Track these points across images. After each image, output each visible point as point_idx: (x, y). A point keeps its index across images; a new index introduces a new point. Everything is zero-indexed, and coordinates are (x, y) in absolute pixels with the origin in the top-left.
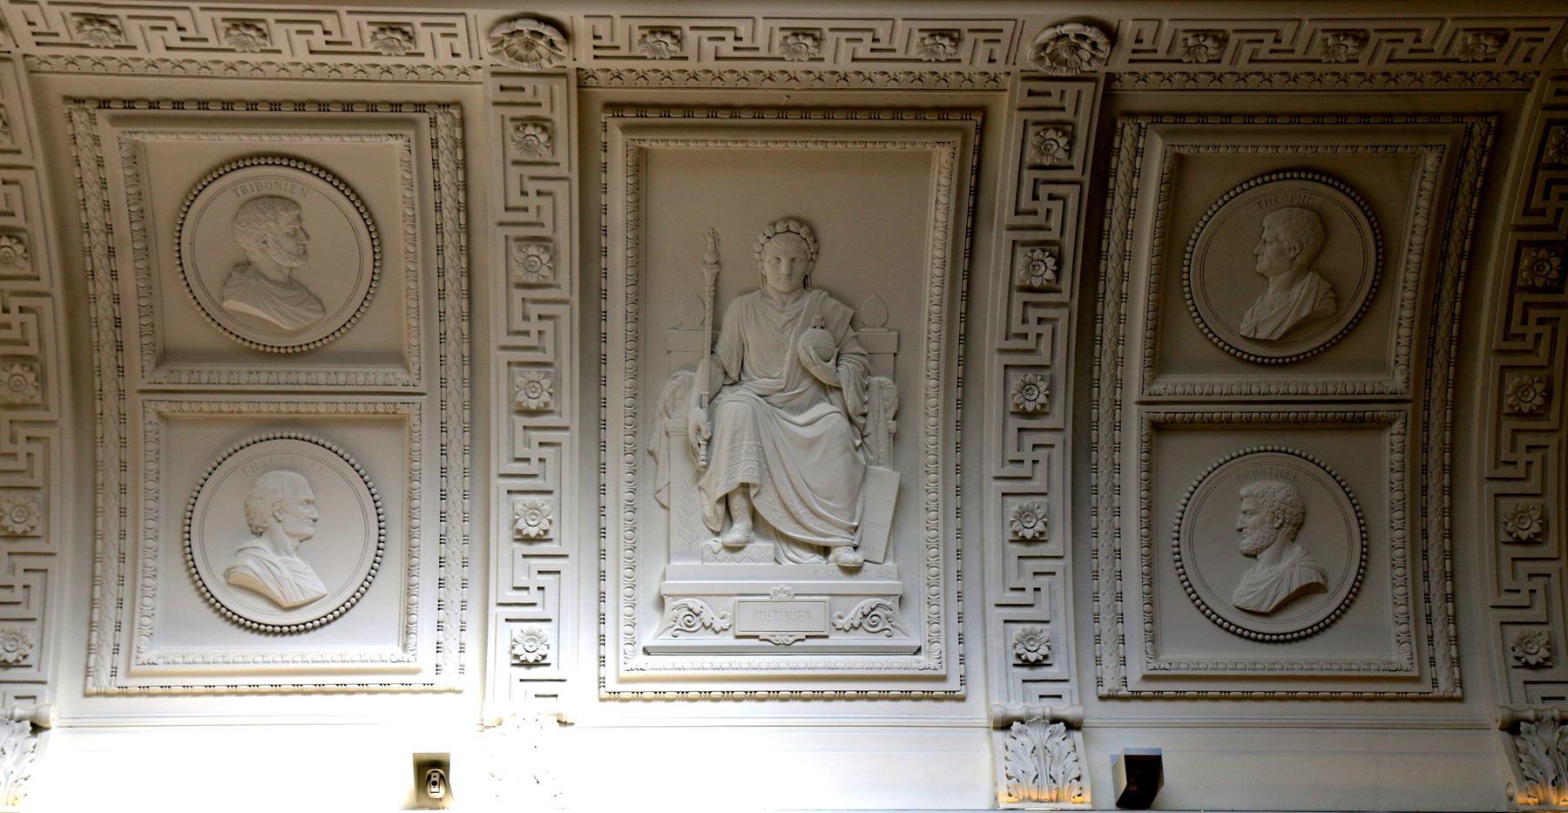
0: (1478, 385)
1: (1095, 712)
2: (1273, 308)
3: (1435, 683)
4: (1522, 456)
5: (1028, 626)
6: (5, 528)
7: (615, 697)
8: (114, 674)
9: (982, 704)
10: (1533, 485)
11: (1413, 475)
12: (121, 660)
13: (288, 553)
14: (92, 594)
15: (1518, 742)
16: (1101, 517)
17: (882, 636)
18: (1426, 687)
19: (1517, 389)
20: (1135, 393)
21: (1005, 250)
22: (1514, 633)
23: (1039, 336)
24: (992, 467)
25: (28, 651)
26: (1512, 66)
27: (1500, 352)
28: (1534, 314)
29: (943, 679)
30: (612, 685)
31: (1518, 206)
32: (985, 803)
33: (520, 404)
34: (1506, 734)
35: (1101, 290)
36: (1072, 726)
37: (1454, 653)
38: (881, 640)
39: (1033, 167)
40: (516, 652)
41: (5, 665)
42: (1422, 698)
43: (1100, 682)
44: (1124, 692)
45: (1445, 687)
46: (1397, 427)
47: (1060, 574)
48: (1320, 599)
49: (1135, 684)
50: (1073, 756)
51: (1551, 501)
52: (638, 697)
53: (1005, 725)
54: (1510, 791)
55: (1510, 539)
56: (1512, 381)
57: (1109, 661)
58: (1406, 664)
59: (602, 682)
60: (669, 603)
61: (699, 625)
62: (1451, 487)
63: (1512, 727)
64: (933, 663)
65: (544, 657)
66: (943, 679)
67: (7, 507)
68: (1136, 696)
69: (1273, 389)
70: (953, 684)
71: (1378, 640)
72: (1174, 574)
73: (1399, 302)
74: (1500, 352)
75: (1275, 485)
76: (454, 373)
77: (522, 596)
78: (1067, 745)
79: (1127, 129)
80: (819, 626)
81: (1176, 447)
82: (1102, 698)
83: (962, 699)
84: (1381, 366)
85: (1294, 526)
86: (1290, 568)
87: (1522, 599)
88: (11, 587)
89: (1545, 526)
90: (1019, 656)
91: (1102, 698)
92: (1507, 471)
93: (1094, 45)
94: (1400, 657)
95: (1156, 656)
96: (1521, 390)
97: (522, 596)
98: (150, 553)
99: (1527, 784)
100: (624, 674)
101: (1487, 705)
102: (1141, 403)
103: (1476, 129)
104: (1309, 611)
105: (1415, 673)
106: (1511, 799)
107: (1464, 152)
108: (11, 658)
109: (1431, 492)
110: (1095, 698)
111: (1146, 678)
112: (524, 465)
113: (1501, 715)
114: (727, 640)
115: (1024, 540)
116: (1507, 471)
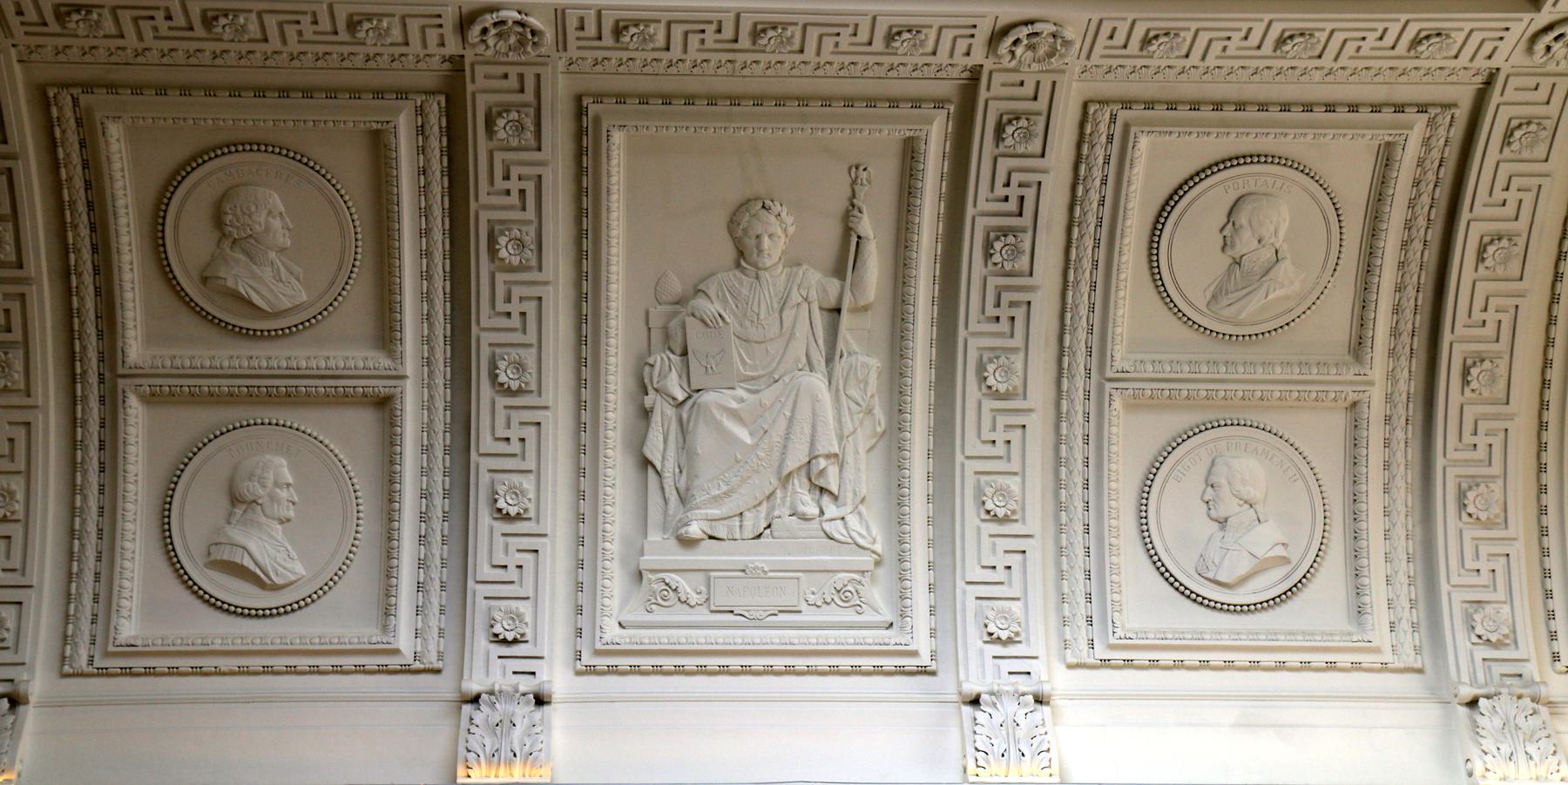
7: (591, 671)
18: (1387, 657)
30: (587, 659)
70: (924, 660)
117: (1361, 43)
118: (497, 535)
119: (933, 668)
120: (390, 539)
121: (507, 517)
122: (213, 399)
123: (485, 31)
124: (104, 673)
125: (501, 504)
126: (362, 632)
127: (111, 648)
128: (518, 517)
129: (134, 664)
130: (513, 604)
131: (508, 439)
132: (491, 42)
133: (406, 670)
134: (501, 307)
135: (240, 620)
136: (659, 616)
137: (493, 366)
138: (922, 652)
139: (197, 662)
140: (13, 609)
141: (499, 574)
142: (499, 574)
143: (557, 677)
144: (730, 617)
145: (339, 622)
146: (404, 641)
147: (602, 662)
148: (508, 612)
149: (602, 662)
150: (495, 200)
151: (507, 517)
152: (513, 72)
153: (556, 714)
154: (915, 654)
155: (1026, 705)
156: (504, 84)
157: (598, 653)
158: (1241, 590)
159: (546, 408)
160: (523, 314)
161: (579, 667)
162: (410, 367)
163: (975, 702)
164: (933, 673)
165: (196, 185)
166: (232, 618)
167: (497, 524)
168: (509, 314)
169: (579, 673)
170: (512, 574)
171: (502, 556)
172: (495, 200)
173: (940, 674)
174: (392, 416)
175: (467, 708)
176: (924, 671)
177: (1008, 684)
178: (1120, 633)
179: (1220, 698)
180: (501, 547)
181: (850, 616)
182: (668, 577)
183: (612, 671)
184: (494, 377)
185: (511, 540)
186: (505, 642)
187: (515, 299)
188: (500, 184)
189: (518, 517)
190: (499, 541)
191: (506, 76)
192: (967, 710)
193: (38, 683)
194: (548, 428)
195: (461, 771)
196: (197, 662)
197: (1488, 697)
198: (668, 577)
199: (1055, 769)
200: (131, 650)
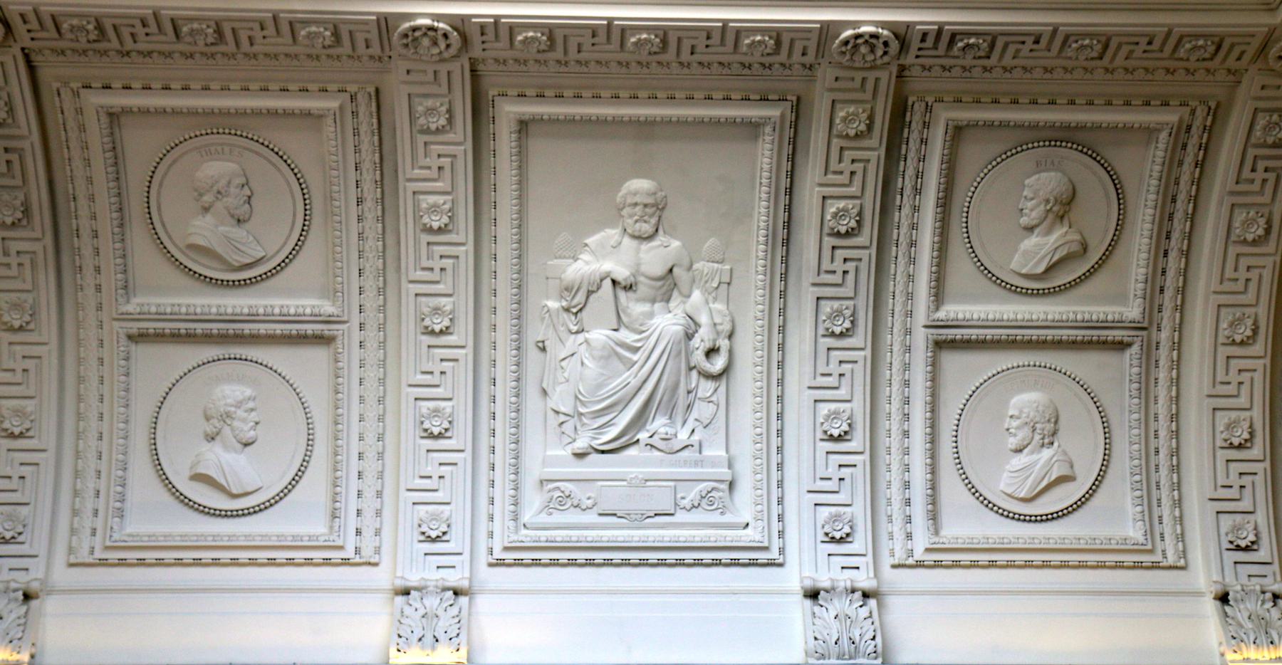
0: (1206, 251)
2: (1012, 474)
4: (1234, 377)
5: (833, 509)
6: (5, 323)
7: (500, 563)
9: (797, 568)
10: (1243, 401)
11: (1167, 186)
16: (893, 456)
18: (1157, 557)
19: (1243, 223)
20: (921, 317)
21: (817, 201)
22: (1226, 522)
23: (852, 173)
24: (809, 276)
26: (1227, 65)
27: (1232, 193)
28: (1261, 165)
29: (766, 549)
30: (498, 554)
31: (1207, 380)
33: (425, 225)
34: (1218, 603)
35: (908, 119)
37: (1177, 513)
38: (715, 518)
39: (840, 136)
41: (6, 542)
42: (1155, 566)
43: (71, 550)
44: (910, 561)
45: (1171, 559)
46: (1135, 349)
47: (860, 467)
49: (919, 554)
50: (870, 621)
51: (1257, 413)
52: (518, 563)
53: (813, 595)
54: (1222, 649)
56: (1240, 217)
58: (1141, 539)
62: (1178, 397)
63: (1224, 598)
64: (758, 537)
66: (766, 549)
67: (5, 413)
68: (919, 565)
69: (1034, 317)
70: (774, 554)
71: (1117, 518)
72: (954, 468)
73: (1137, 247)
74: (1232, 193)
75: (1053, 174)
76: (368, 177)
77: (426, 483)
78: (864, 612)
79: (916, 106)
81: (953, 362)
84: (1121, 298)
85: (1049, 430)
87: (1233, 493)
88: (13, 370)
90: (827, 534)
91: (894, 566)
92: (1222, 390)
93: (886, 44)
94: (1135, 532)
95: (937, 533)
96: (1247, 223)
97: (426, 483)
99: (1233, 642)
101: (1204, 574)
102: (926, 327)
103: (1199, 112)
105: (1149, 547)
106: (1222, 655)
107: (1189, 128)
108: (8, 535)
109: (1189, 148)
111: (927, 550)
112: (429, 377)
113: (1218, 589)
115: (832, 438)
116: (1222, 390)
117: (1020, 46)
119: (781, 561)
122: (208, 338)
124: (103, 563)
126: (316, 527)
135: (213, 520)
136: (558, 518)
139: (290, 554)
144: (614, 519)
145: (301, 519)
147: (113, 556)
150: (418, 172)
154: (341, 548)
155: (448, 599)
156: (850, 85)
163: (406, 592)
164: (781, 565)
168: (845, 272)
172: (418, 172)
173: (787, 565)
178: (116, 536)
181: (715, 518)
191: (853, 79)
196: (290, 554)
197: (827, 591)
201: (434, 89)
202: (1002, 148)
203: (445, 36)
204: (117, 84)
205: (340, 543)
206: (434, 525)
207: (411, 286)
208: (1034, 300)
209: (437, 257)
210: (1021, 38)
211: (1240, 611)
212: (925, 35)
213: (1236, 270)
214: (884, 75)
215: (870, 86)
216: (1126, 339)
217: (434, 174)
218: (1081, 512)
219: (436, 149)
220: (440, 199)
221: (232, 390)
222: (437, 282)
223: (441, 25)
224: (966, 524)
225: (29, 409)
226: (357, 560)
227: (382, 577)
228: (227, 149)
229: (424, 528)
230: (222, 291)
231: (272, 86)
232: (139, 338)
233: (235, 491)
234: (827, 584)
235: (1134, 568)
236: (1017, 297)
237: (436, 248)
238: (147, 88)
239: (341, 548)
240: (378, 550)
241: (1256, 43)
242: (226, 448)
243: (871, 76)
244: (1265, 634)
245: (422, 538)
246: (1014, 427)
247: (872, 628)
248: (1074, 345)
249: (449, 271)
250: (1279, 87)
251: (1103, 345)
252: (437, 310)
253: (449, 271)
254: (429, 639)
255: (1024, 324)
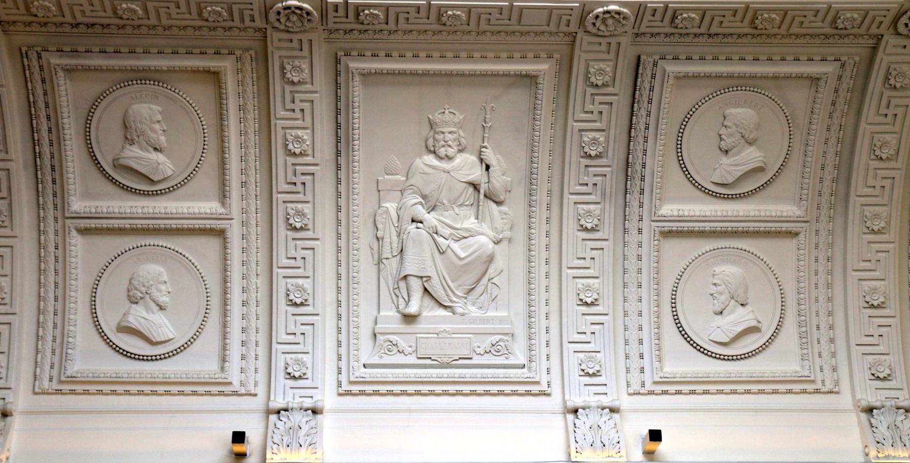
1: (625, 402)
3: (823, 382)
7: (349, 393)
8: (51, 380)
12: (59, 214)
13: (153, 313)
14: (39, 293)
15: (873, 420)
17: (503, 357)
18: (819, 385)
25: (4, 296)
30: (345, 387)
32: (562, 457)
36: (613, 410)
40: (289, 371)
42: (817, 391)
43: (628, 385)
48: (758, 335)
55: (867, 305)
57: (635, 372)
59: (339, 384)
60: (380, 338)
61: (395, 351)
65: (304, 374)
70: (544, 387)
78: (611, 423)
80: (465, 352)
82: (630, 394)
83: (549, 395)
86: (738, 319)
89: (888, 223)
98: (73, 299)
100: (352, 379)
104: (755, 183)
110: (626, 395)
114: (412, 360)
118: (290, 239)
120: (226, 270)
121: (295, 229)
123: (279, 13)
125: (291, 221)
127: (63, 378)
128: (302, 229)
129: (72, 385)
130: (300, 206)
131: (295, 184)
132: (283, 20)
133: (235, 394)
134: (289, 105)
135: (137, 362)
137: (283, 68)
138: (542, 382)
140: (6, 327)
141: (291, 338)
142: (291, 338)
143: (327, 398)
144: (429, 362)
145: (200, 363)
146: (234, 376)
147: (355, 388)
148: (297, 360)
149: (355, 388)
151: (295, 229)
152: (295, 37)
153: (326, 421)
154: (538, 383)
156: (597, 48)
157: (351, 383)
158: (733, 346)
159: (318, 239)
160: (302, 110)
161: (340, 391)
162: (235, 212)
165: (97, 136)
166: (133, 361)
167: (289, 233)
168: (294, 110)
169: (340, 395)
170: (299, 263)
171: (293, 252)
174: (225, 239)
175: (273, 418)
176: (543, 394)
177: (594, 401)
179: (717, 410)
180: (293, 323)
182: (391, 337)
183: (362, 393)
184: (283, 74)
185: (298, 242)
186: (294, 378)
187: (297, 101)
188: (289, 105)
189: (302, 229)
190: (291, 244)
192: (570, 417)
193: (20, 399)
194: (319, 251)
195: (269, 455)
196: (208, 388)
197: (584, 409)
198: (391, 337)
199: (623, 453)
200: (72, 380)
201: (606, 56)
202: (709, 91)
203: (308, 13)
204: (696, 57)
205: (537, 379)
206: (591, 365)
207: (571, 197)
208: (728, 201)
209: (591, 175)
210: (723, 13)
211: (882, 421)
212: (655, 10)
213: (303, 174)
214: (624, 40)
215: (613, 47)
216: (794, 230)
217: (595, 116)
218: (761, 356)
219: (598, 99)
220: (597, 135)
221: (153, 271)
222: (590, 194)
223: (625, 10)
224: (684, 363)
225: (596, 286)
226: (243, 392)
227: (845, 400)
228: (138, 95)
229: (583, 367)
230: (135, 197)
231: (223, 51)
232: (668, 234)
233: (726, 340)
234: (878, 404)
235: (758, 393)
236: (712, 199)
237: (590, 169)
238: (689, 58)
239: (538, 383)
240: (837, 383)
241: (890, 17)
242: (148, 309)
243: (614, 41)
244: (899, 440)
245: (582, 373)
246: (722, 291)
247: (617, 436)
248: (768, 234)
249: (887, 189)
250: (905, 47)
251: (778, 234)
252: (876, 216)
253: (887, 189)
254: (598, 444)
255: (733, 219)
